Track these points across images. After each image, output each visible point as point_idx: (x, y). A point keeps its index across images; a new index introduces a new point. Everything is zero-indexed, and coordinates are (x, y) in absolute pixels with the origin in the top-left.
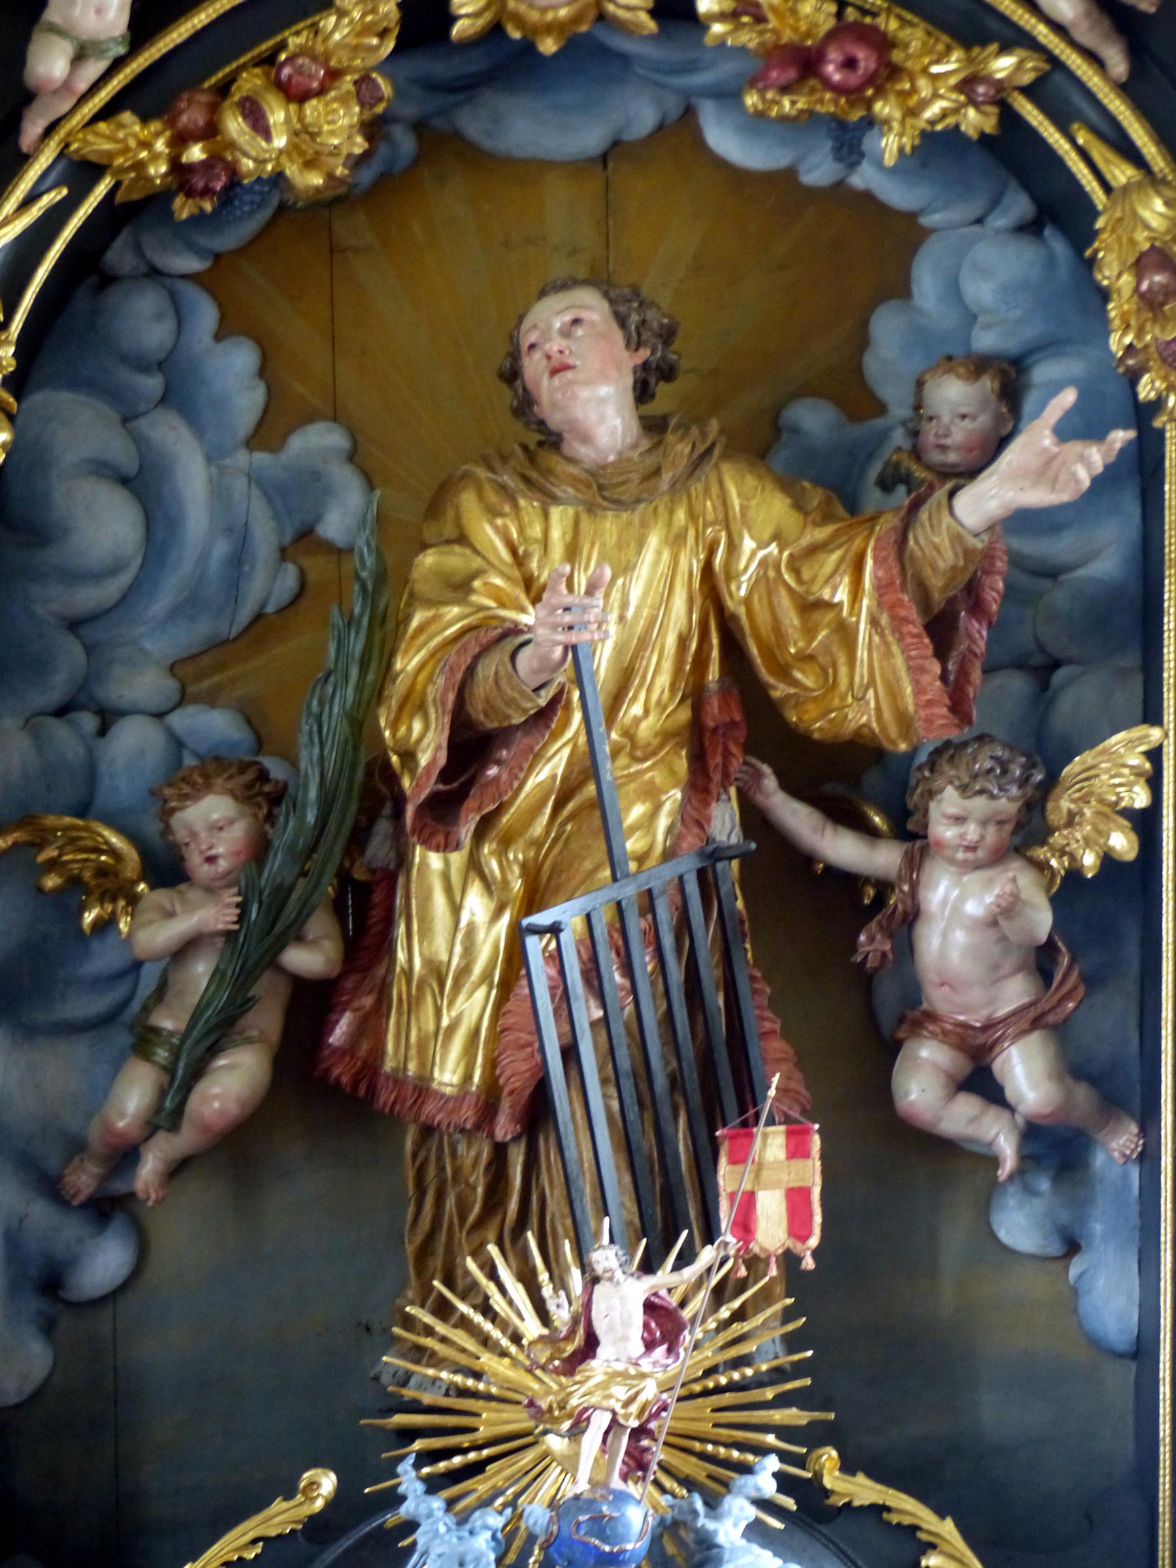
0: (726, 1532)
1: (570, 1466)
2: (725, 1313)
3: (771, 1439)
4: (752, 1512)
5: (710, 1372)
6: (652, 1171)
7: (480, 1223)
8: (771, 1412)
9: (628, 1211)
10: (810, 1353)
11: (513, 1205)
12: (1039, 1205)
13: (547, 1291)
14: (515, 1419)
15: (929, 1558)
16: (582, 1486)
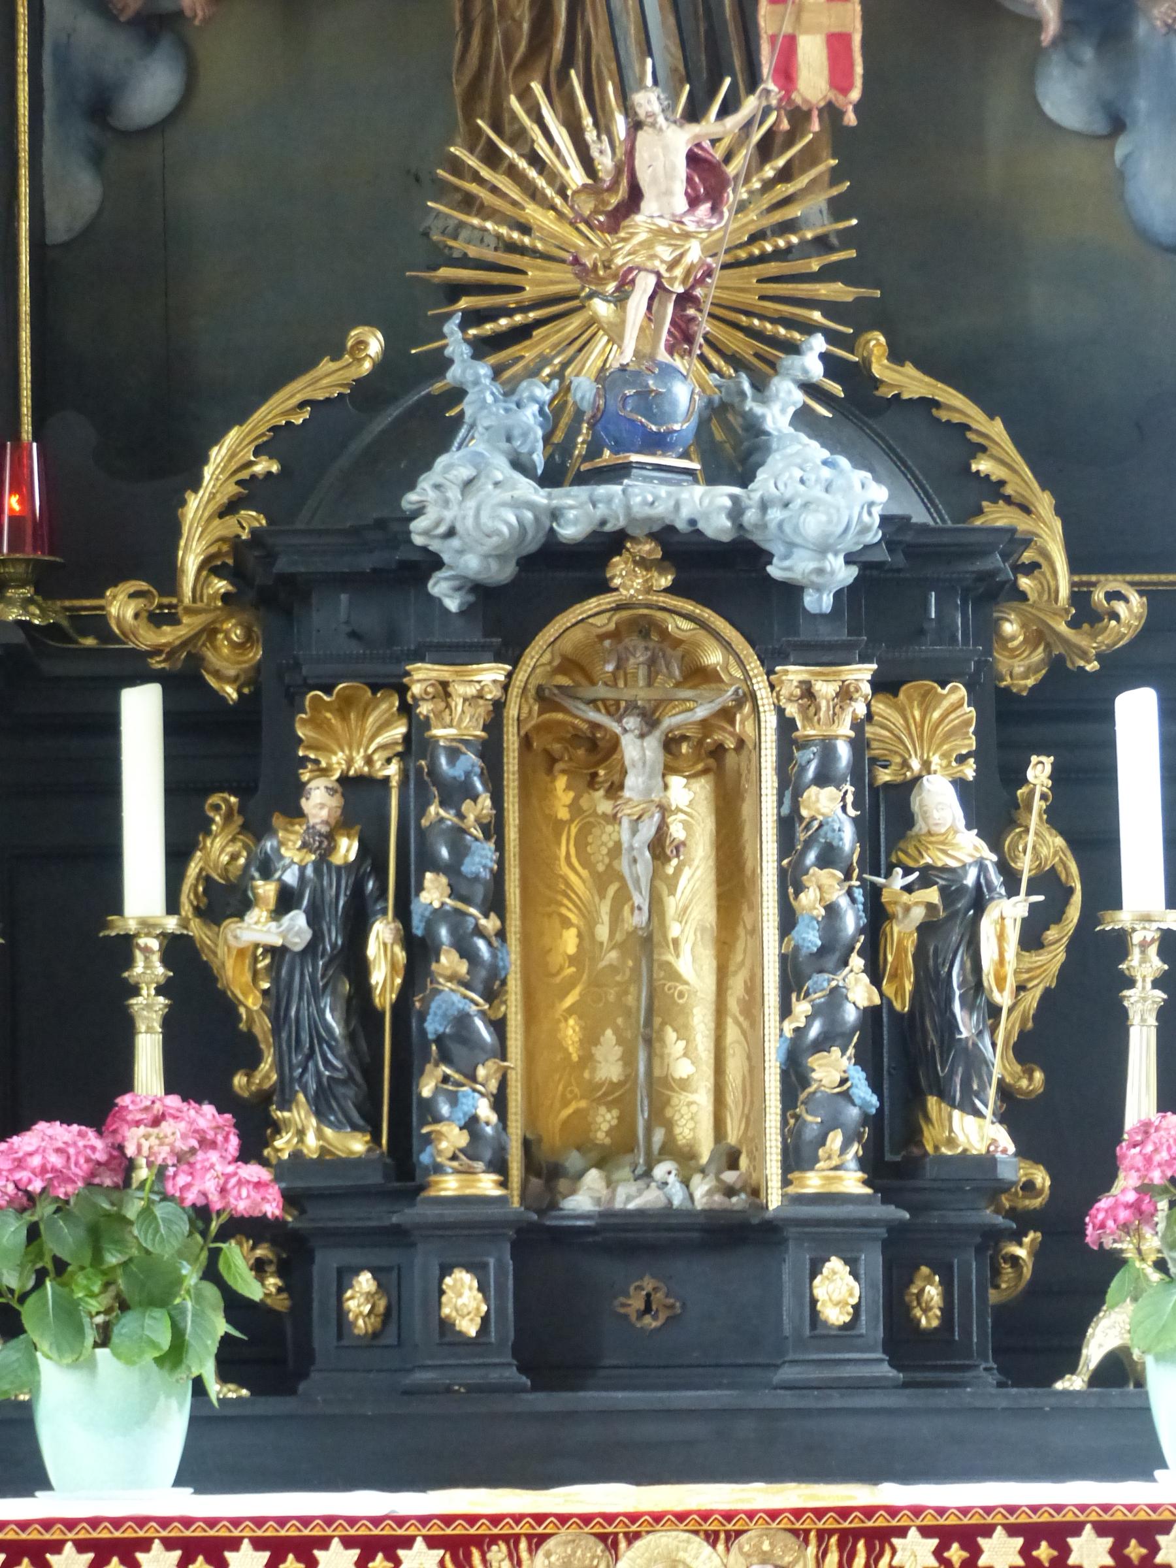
0: (773, 417)
1: (616, 337)
2: (769, 172)
3: (817, 315)
4: (799, 397)
5: (755, 238)
6: (696, 12)
7: (525, 66)
8: (818, 286)
9: (672, 55)
10: (854, 222)
11: (559, 44)
12: (1082, 76)
13: (590, 135)
14: (561, 279)
15: (978, 463)
16: (627, 357)
